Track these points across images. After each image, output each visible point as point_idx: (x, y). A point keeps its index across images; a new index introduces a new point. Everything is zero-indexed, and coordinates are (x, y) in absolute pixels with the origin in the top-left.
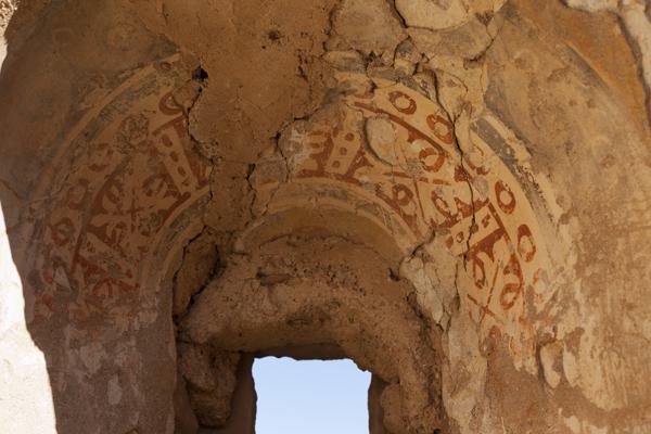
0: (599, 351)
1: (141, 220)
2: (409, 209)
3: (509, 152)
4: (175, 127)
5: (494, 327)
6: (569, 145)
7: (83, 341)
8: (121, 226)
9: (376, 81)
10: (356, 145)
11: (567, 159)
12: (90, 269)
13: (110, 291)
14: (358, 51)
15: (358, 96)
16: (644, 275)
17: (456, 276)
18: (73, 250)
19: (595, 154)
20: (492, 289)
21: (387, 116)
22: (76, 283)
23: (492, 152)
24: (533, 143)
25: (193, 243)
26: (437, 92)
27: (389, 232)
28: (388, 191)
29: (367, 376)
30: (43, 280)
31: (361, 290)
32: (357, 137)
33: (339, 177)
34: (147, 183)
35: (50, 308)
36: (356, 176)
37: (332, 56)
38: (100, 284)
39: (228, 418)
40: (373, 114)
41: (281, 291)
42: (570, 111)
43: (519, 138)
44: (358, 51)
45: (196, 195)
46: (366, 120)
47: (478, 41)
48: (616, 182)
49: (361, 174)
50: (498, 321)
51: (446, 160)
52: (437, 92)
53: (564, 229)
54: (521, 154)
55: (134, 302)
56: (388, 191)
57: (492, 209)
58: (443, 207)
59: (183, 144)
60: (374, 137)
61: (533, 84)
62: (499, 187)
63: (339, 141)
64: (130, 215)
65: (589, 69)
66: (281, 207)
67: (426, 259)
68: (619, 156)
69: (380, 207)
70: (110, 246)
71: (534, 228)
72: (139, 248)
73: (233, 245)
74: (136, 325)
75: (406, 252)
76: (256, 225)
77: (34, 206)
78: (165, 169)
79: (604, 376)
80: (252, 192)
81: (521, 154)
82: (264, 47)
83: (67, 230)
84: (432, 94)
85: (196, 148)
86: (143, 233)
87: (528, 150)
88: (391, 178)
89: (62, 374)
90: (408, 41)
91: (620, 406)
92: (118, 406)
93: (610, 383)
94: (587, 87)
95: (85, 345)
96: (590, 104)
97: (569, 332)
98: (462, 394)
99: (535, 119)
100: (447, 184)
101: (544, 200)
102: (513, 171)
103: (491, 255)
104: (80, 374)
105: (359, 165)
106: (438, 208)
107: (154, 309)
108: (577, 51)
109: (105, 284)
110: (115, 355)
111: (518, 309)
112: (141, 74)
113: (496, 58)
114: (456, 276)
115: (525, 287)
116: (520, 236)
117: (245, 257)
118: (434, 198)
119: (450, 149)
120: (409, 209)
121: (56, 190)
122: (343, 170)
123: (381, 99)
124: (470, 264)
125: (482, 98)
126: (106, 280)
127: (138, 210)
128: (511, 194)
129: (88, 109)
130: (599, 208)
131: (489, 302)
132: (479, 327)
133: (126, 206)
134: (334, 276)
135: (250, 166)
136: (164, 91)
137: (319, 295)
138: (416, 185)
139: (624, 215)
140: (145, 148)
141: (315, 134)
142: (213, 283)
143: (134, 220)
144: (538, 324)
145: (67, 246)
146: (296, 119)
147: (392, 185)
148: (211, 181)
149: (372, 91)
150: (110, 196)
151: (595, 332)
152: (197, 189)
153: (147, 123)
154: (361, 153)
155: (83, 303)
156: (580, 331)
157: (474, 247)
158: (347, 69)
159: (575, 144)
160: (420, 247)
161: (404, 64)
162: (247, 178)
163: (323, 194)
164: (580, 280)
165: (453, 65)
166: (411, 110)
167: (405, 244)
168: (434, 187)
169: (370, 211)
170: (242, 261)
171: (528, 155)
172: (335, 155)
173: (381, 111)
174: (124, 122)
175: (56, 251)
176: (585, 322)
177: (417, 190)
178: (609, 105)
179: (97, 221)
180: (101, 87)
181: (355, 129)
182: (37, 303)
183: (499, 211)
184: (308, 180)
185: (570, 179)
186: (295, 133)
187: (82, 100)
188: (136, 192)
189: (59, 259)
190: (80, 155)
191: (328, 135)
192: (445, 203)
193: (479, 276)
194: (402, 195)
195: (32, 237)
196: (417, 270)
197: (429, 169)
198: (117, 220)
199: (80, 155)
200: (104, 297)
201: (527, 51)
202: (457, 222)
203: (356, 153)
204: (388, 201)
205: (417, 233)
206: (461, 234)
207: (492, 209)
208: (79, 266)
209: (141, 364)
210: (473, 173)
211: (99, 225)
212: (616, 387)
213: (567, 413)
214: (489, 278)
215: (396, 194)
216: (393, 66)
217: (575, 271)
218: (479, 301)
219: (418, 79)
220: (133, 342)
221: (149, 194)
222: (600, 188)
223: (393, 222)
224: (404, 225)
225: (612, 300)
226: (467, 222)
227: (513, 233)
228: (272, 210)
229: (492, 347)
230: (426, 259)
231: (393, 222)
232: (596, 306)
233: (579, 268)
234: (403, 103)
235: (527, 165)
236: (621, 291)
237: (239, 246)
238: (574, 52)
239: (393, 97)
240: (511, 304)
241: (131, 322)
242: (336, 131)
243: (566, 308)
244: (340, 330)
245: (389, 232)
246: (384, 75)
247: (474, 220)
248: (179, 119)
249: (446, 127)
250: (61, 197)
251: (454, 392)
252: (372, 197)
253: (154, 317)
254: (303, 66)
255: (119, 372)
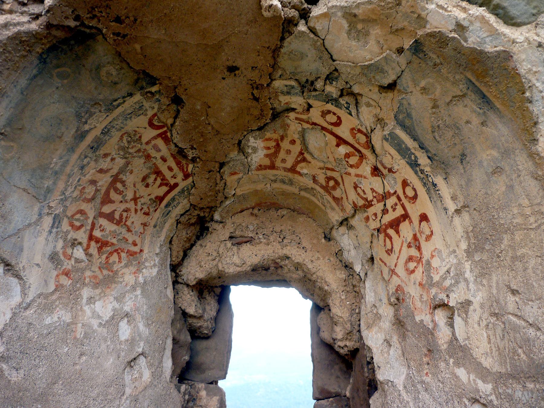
0: (485, 323)
1: (142, 204)
2: (337, 193)
3: (413, 158)
4: (163, 138)
5: (399, 285)
6: (463, 155)
7: (97, 298)
8: (127, 210)
9: (311, 102)
10: (296, 149)
11: (461, 167)
12: (102, 244)
13: (120, 258)
14: (296, 80)
15: (298, 113)
16: (526, 269)
17: (371, 242)
18: (88, 232)
19: (485, 164)
20: (398, 257)
21: (319, 127)
22: (91, 255)
23: (400, 157)
24: (434, 152)
25: (183, 217)
26: (357, 110)
27: (323, 208)
28: (322, 179)
29: (308, 304)
30: (62, 258)
31: (303, 248)
32: (298, 142)
33: (285, 169)
34: (144, 179)
35: (69, 277)
36: (298, 169)
37: (278, 84)
38: (111, 254)
39: (213, 332)
40: (311, 127)
41: (246, 249)
42: (466, 129)
43: (422, 148)
44: (296, 80)
45: (182, 185)
46: (304, 130)
47: (390, 72)
48: (504, 189)
49: (302, 168)
50: (402, 281)
51: (364, 161)
52: (357, 110)
53: (457, 220)
54: (423, 160)
55: (139, 263)
56: (322, 179)
57: (399, 199)
58: (362, 194)
59: (169, 150)
60: (311, 142)
61: (435, 106)
62: (405, 184)
63: (285, 145)
64: (133, 202)
65: (484, 96)
66: (244, 190)
67: (351, 228)
68: (507, 169)
69: (315, 190)
70: (118, 225)
71: (431, 215)
72: (142, 224)
73: (212, 216)
74: (141, 280)
75: (335, 223)
76: (228, 203)
77: (52, 204)
78: (158, 168)
79: (489, 342)
80: (223, 181)
81: (423, 160)
82: (224, 79)
83: (82, 218)
84: (354, 112)
85: (181, 152)
86: (144, 213)
87: (429, 158)
88: (324, 171)
89: (80, 325)
90: (335, 72)
91: (503, 371)
92: (127, 341)
93: (494, 349)
94: (481, 111)
95: (99, 300)
96: (483, 124)
97: (459, 301)
98: (375, 329)
99: (436, 134)
100: (365, 178)
101: (440, 197)
102: (416, 173)
103: (398, 232)
104: (95, 323)
105: (300, 162)
106: (358, 194)
107: (155, 265)
108: (474, 80)
109: (115, 254)
110: (124, 303)
111: (418, 275)
112: (130, 102)
113: (405, 85)
114: (371, 242)
115: (424, 260)
116: (421, 221)
117: (221, 225)
118: (356, 187)
119: (367, 152)
120: (337, 193)
121: (70, 190)
122: (289, 165)
123: (315, 115)
124: (382, 236)
125: (393, 116)
126: (116, 251)
127: (139, 198)
128: (415, 190)
129: (91, 129)
130: (488, 208)
131: (395, 266)
132: (387, 282)
133: (130, 195)
134: (284, 238)
135: (220, 163)
136: (150, 113)
137: (273, 252)
138: (342, 177)
139: (510, 216)
140: (141, 154)
141: (267, 140)
142: (199, 243)
143: (136, 205)
144: (433, 291)
145: (83, 229)
146: (252, 130)
147: (325, 176)
148: (193, 174)
149: (308, 110)
150: (116, 190)
151: (482, 306)
152: (183, 180)
153: (140, 137)
154: (301, 153)
155: (97, 269)
156: (468, 303)
157: (385, 224)
158: (288, 93)
159: (468, 156)
160: (346, 219)
161: (332, 90)
162: (219, 172)
163: (275, 181)
164: (470, 262)
165: (370, 90)
166: (338, 123)
167: (335, 217)
168: (356, 179)
169: (309, 193)
170: (219, 227)
171: (429, 161)
172: (282, 155)
173: (315, 124)
174: (122, 136)
175: (72, 235)
176: (474, 296)
177: (343, 180)
178: (500, 126)
179: (107, 209)
180: (100, 111)
181: (296, 136)
182: (57, 276)
183: (404, 200)
184: (264, 172)
185: (463, 183)
186: (252, 140)
187: (86, 123)
188: (136, 185)
189: (76, 240)
190: (88, 163)
191: (277, 141)
192: (364, 191)
193: (389, 246)
194: (332, 183)
195: (52, 227)
196: (343, 235)
197: (351, 166)
198: (123, 206)
199: (88, 163)
200: (114, 263)
201: (431, 81)
202: (373, 205)
203: (297, 154)
204: (322, 187)
205: (343, 210)
206: (375, 215)
207: (399, 199)
208: (93, 243)
209: (145, 307)
210: (385, 172)
211: (108, 212)
212: (500, 354)
213: (457, 364)
214: (396, 248)
215: (328, 183)
216: (323, 91)
217: (465, 255)
218: (388, 264)
219: (342, 101)
220: (139, 292)
221: (147, 186)
222: (489, 192)
223: (325, 201)
224: (334, 204)
225: (497, 283)
226: (380, 206)
227: (415, 217)
228: (239, 192)
229: (398, 300)
230: (351, 228)
231: (325, 201)
232: (483, 285)
233: (469, 253)
234: (332, 118)
235: (427, 169)
236: (506, 277)
237: (217, 217)
238: (471, 81)
239: (324, 114)
240: (413, 272)
241: (137, 278)
242: (282, 138)
243: (457, 282)
244: (288, 275)
245: (323, 208)
246: (316, 98)
247: (385, 205)
248: (165, 132)
249: (364, 137)
250: (75, 194)
251: (369, 327)
252: (310, 183)
253: (155, 271)
254: (255, 92)
255: (127, 315)
